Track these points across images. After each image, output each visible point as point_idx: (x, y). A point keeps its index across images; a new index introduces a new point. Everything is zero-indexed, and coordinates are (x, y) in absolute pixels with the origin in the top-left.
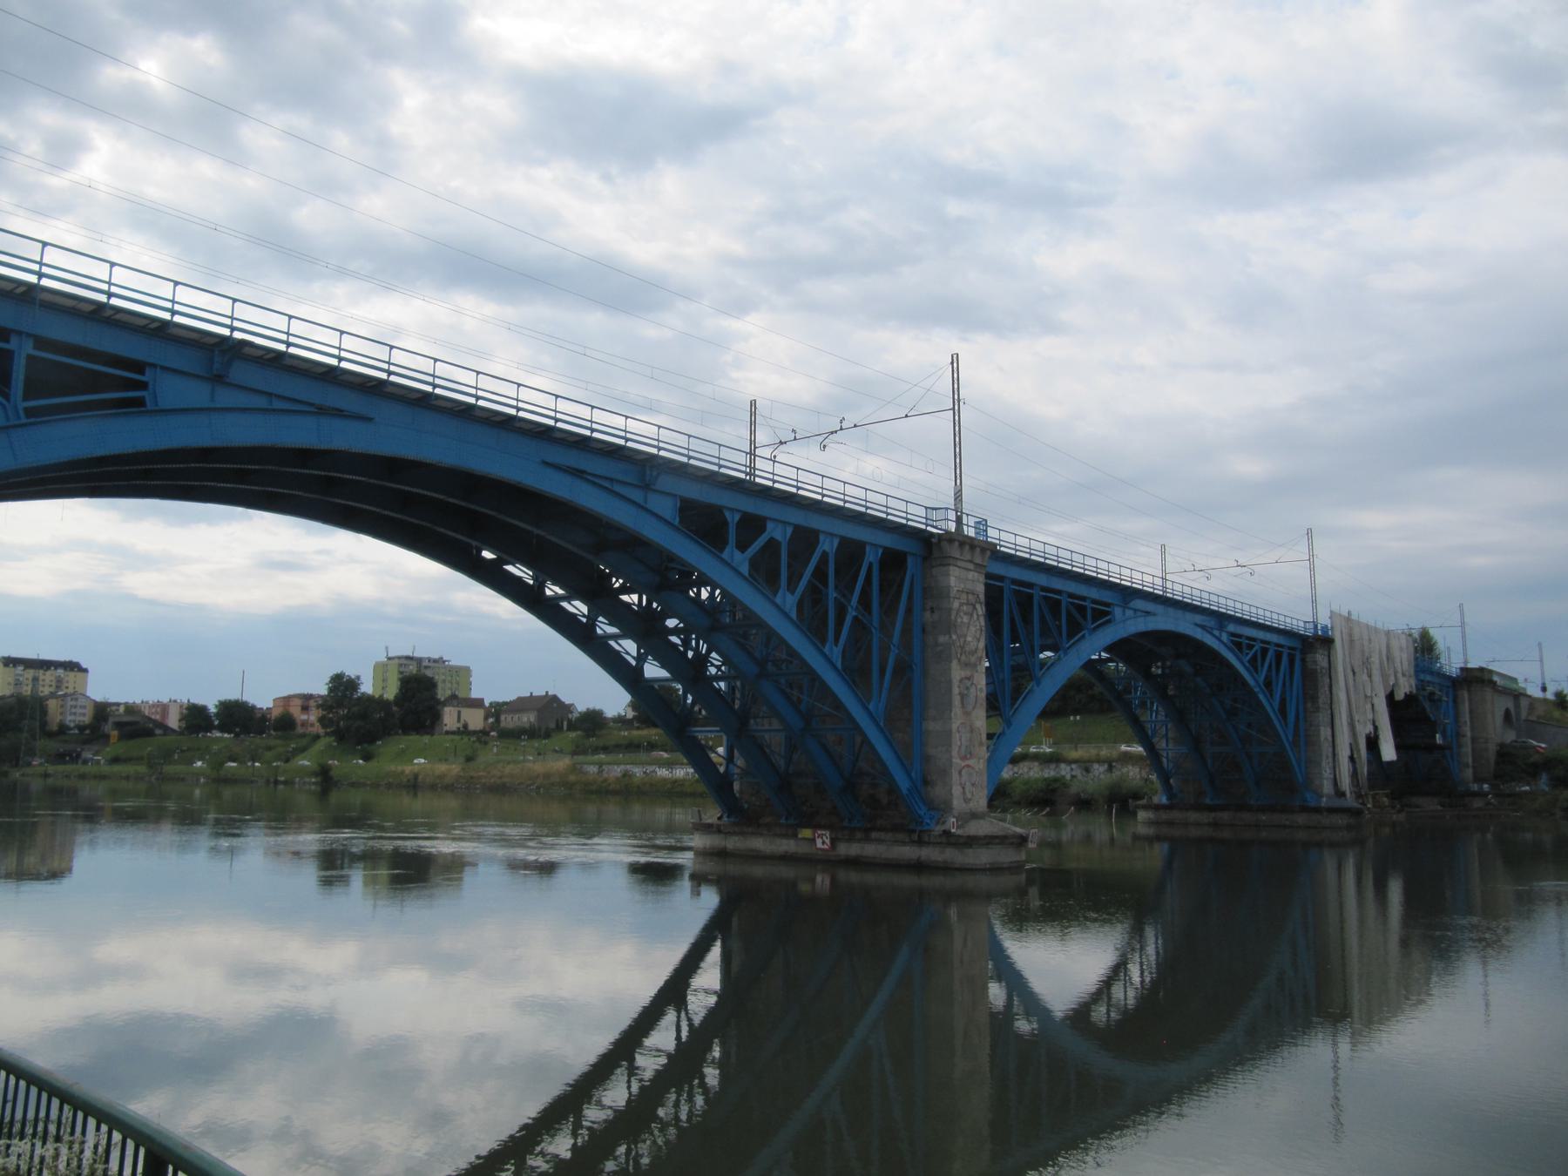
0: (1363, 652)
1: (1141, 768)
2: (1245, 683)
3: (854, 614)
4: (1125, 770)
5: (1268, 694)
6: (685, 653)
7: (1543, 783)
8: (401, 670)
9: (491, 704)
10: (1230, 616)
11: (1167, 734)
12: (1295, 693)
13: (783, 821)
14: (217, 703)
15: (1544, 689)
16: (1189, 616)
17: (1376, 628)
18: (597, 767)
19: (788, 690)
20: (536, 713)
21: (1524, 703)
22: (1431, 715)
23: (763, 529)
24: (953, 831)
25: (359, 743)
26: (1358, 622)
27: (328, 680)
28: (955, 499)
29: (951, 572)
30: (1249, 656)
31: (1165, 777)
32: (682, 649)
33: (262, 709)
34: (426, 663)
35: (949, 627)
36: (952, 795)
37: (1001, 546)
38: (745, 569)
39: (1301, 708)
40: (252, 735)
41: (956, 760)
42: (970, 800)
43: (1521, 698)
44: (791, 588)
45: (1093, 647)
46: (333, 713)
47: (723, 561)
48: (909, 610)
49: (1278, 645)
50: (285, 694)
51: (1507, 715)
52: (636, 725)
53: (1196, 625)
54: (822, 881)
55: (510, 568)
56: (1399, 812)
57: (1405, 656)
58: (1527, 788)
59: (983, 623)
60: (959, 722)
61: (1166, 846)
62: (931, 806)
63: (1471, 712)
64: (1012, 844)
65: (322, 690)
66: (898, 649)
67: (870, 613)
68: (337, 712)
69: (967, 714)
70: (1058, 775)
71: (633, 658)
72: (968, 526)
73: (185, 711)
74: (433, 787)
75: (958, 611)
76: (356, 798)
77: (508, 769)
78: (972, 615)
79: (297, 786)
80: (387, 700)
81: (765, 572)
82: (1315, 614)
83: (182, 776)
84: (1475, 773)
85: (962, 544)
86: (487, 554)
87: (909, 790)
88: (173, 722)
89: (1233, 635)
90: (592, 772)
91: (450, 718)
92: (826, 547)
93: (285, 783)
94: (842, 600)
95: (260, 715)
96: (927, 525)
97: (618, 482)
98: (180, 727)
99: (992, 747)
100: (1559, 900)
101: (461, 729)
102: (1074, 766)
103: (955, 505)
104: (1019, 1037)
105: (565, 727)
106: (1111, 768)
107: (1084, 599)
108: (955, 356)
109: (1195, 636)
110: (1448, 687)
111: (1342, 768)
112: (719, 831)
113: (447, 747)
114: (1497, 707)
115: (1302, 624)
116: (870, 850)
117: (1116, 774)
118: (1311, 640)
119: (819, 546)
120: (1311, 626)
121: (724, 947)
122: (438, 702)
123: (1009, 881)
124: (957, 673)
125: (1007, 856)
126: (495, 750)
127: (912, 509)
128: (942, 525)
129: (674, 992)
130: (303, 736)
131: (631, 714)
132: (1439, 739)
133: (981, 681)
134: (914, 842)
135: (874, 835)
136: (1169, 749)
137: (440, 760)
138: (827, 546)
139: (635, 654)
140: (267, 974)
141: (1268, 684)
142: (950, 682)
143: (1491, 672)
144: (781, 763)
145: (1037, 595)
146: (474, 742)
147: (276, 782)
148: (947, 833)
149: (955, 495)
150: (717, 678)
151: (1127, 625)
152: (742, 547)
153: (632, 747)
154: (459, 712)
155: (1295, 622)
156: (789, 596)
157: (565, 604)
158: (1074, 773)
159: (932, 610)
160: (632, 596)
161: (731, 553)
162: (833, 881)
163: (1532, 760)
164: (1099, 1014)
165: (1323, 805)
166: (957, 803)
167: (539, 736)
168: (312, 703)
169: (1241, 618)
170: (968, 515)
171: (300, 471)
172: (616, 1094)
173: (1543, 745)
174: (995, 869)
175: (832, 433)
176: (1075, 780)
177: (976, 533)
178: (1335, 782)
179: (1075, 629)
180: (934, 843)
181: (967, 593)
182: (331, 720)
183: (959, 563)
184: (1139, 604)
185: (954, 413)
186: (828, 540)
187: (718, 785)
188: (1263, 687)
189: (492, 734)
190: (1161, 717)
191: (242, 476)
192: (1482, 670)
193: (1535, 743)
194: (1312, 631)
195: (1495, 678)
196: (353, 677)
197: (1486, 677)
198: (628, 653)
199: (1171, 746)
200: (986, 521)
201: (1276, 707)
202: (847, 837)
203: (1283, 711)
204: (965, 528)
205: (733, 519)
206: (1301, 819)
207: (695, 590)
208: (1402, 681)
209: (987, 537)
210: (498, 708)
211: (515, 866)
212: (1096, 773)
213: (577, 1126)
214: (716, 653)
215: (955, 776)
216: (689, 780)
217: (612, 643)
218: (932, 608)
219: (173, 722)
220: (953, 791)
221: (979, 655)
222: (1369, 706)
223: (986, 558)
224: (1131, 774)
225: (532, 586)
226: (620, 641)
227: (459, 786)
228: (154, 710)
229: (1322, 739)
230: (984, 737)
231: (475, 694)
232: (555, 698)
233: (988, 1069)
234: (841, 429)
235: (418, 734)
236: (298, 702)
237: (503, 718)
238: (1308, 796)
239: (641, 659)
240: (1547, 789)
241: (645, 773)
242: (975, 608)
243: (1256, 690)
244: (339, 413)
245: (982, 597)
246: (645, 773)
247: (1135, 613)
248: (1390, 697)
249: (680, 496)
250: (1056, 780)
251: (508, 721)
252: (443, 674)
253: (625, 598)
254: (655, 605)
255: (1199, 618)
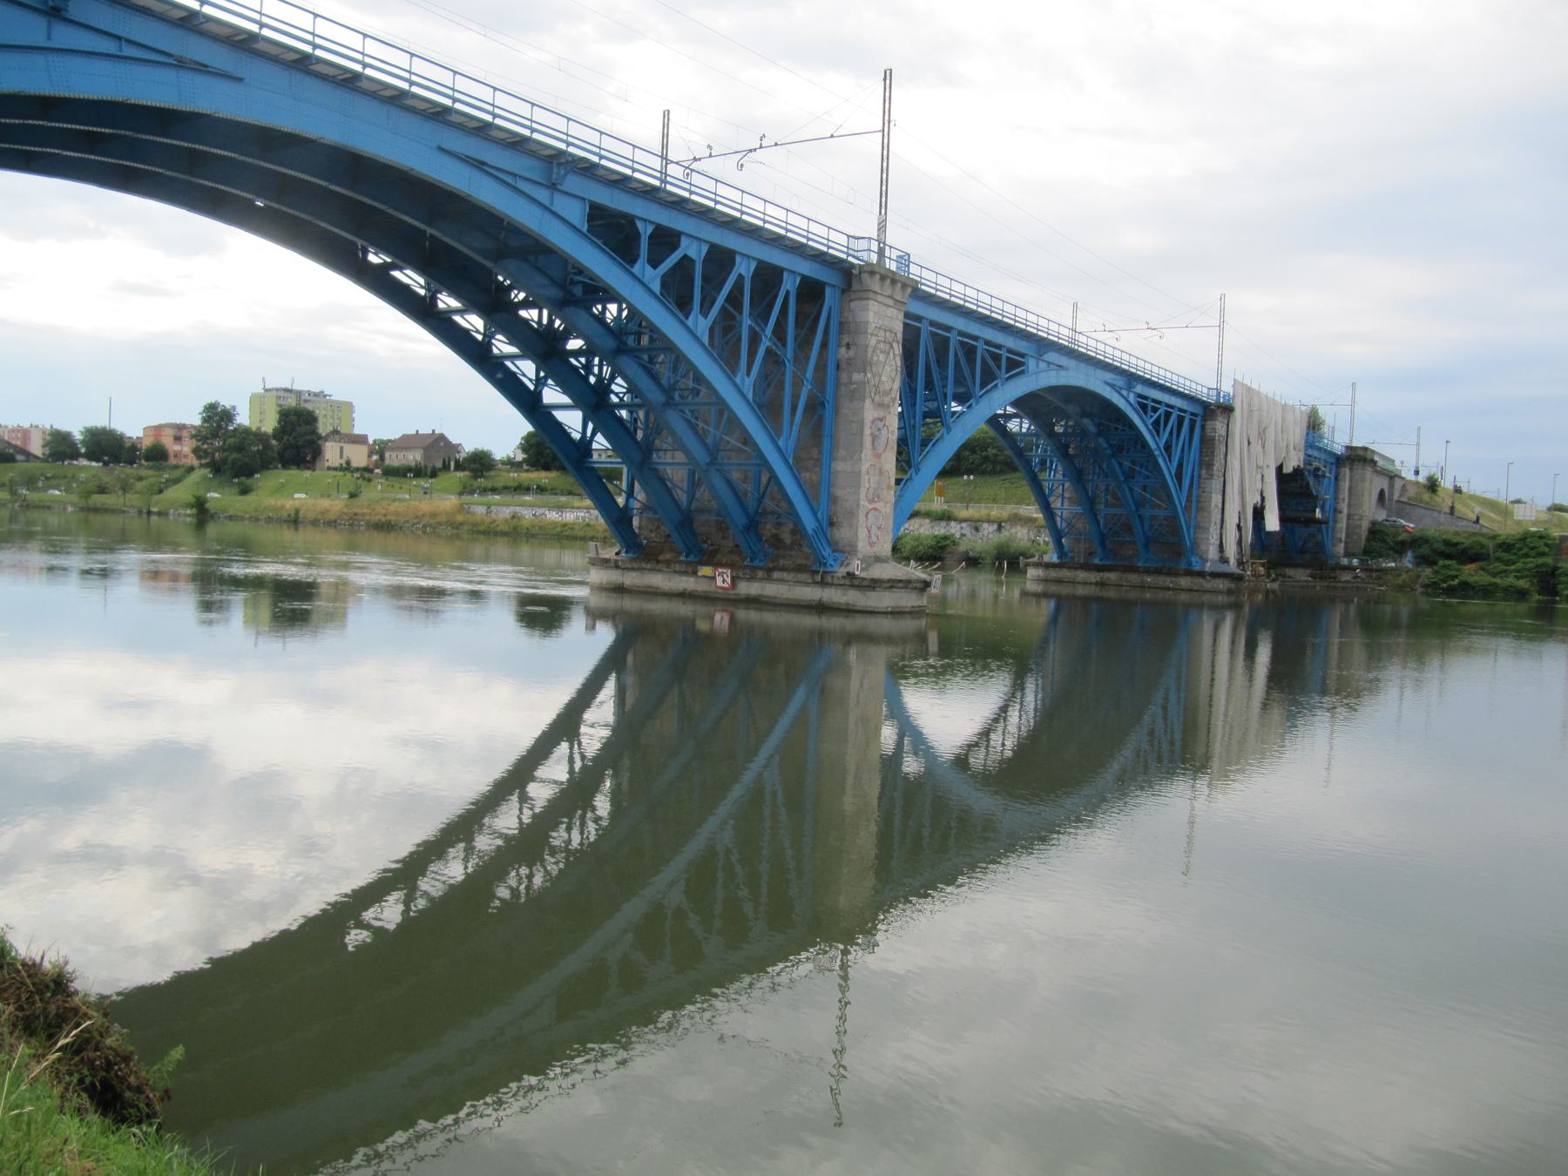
0: (1260, 422)
1: (1029, 530)
2: (1145, 445)
3: (768, 344)
4: (1013, 531)
5: (1166, 456)
6: (586, 379)
7: (1408, 560)
8: (279, 402)
9: (375, 441)
10: (1139, 376)
11: (1063, 494)
12: (1191, 460)
13: (682, 558)
14: (83, 430)
15: (1417, 473)
16: (1100, 373)
17: (1274, 400)
18: (485, 508)
19: (693, 420)
20: (422, 451)
21: (1398, 484)
22: (1314, 491)
23: (675, 246)
24: (857, 573)
25: (237, 476)
26: (1259, 393)
27: (201, 409)
28: (879, 230)
29: (870, 307)
30: (1153, 419)
31: (1057, 536)
32: (582, 372)
33: (131, 438)
34: (306, 396)
35: (864, 366)
36: (857, 537)
37: (922, 284)
38: (656, 287)
39: (1196, 474)
40: (121, 465)
41: (863, 502)
42: (875, 543)
43: (1396, 479)
44: (705, 311)
45: (1000, 399)
46: (208, 444)
47: (634, 276)
48: (824, 345)
49: (1181, 410)
50: (156, 423)
51: (1382, 494)
52: (525, 467)
53: (1106, 383)
54: (721, 620)
55: (396, 274)
56: (1274, 580)
57: (1298, 430)
58: (1393, 564)
59: (899, 364)
60: (869, 464)
61: (1052, 604)
62: (836, 548)
63: (1350, 489)
64: (915, 588)
65: (195, 420)
66: (811, 384)
67: (784, 344)
68: (212, 444)
69: (878, 456)
70: (948, 533)
71: (531, 380)
72: (890, 258)
73: (48, 438)
74: (314, 523)
75: (875, 348)
76: (235, 529)
77: (394, 507)
78: (888, 353)
79: (171, 517)
80: (265, 432)
81: (678, 292)
82: (1219, 381)
83: (48, 504)
84: (1346, 548)
85: (883, 278)
86: (374, 259)
87: (814, 530)
88: (36, 448)
89: (1140, 396)
90: (480, 513)
91: (332, 453)
92: (743, 271)
93: (159, 514)
94: (757, 329)
95: (130, 444)
96: (848, 255)
97: (522, 177)
98: (44, 454)
99: (898, 493)
100: (1563, 633)
101: (344, 465)
102: (964, 525)
103: (878, 236)
104: (906, 777)
105: (452, 467)
106: (1000, 528)
107: (999, 347)
108: (888, 72)
109: (1104, 395)
110: (1332, 464)
111: (1228, 536)
112: (617, 567)
113: (329, 483)
114: (1373, 485)
115: (1205, 391)
116: (771, 590)
117: (1005, 534)
118: (1212, 407)
119: (736, 268)
120: (1215, 392)
121: (618, 679)
122: (320, 437)
123: (909, 625)
124: (870, 413)
125: (908, 600)
126: (380, 487)
127: (834, 236)
128: (864, 256)
129: (567, 725)
130: (176, 467)
131: (520, 456)
132: (1318, 514)
133: (894, 423)
134: (817, 583)
135: (776, 575)
136: (1064, 508)
137: (322, 496)
138: (744, 268)
139: (534, 377)
140: (141, 706)
141: (1168, 448)
142: (861, 423)
143: (1373, 452)
144: (683, 498)
145: (954, 339)
146: (358, 478)
147: (149, 513)
148: (850, 575)
149: (879, 225)
150: (621, 405)
151: (1038, 378)
152: (654, 263)
153: (522, 489)
154: (342, 448)
155: (1199, 388)
156: (701, 318)
157: (457, 318)
158: (964, 532)
159: (848, 346)
160: (530, 311)
161: (641, 267)
162: (732, 620)
163: (1400, 538)
164: (977, 760)
165: (1207, 569)
166: (862, 546)
167: (425, 475)
168: (185, 433)
169: (1149, 379)
170: (891, 247)
171: (158, 139)
172: (508, 819)
173: (1412, 525)
174: (896, 613)
175: (751, 151)
176: (965, 538)
177: (897, 268)
178: (1221, 547)
179: (988, 377)
180: (836, 585)
181: (885, 330)
182: (205, 451)
183: (880, 298)
184: (1052, 357)
185: (883, 135)
186: (744, 262)
187: (619, 520)
188: (1163, 450)
189: (377, 471)
190: (1059, 476)
191: (91, 142)
192: (1365, 449)
193: (1404, 522)
194: (1215, 398)
195: (1376, 458)
196: (228, 407)
197: (1369, 457)
198: (524, 375)
199: (1066, 506)
200: (909, 255)
201: (1173, 472)
202: (748, 576)
203: (1179, 476)
204: (887, 260)
205: (645, 231)
206: (1184, 582)
207: (599, 307)
208: (1293, 453)
209: (909, 273)
210: (382, 445)
211: (397, 592)
212: (985, 532)
213: (470, 850)
214: (622, 378)
215: (862, 517)
216: (580, 524)
217: (508, 364)
218: (848, 344)
219: (36, 448)
220: (859, 534)
221: (893, 396)
222: (1259, 476)
223: (907, 295)
224: (1019, 535)
225: (425, 297)
226: (516, 362)
227: (343, 522)
228: (14, 435)
229: (1213, 506)
230: (893, 482)
231: (357, 431)
232: (442, 437)
233: (876, 804)
234: (761, 147)
235: (298, 468)
236: (171, 432)
237: (387, 455)
238: (1194, 559)
239: (540, 383)
240: (1410, 566)
241: (534, 515)
242: (892, 347)
243: (1157, 453)
244: (202, 68)
245: (900, 336)
246: (534, 515)
247: (1048, 367)
248: (1279, 469)
249: (589, 201)
250: (945, 538)
251: (394, 459)
252: (324, 409)
253: (523, 313)
254: (557, 323)
255: (1109, 376)
